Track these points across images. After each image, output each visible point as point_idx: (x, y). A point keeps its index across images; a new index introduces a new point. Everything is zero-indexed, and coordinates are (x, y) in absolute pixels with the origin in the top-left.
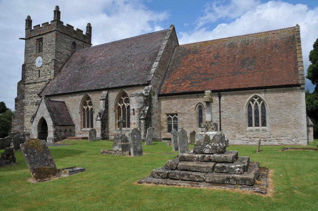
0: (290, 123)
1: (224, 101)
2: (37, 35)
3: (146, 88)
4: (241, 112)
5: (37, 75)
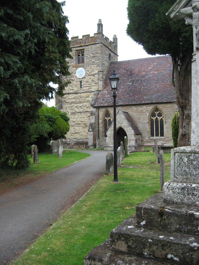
2: (76, 46)
5: (78, 86)
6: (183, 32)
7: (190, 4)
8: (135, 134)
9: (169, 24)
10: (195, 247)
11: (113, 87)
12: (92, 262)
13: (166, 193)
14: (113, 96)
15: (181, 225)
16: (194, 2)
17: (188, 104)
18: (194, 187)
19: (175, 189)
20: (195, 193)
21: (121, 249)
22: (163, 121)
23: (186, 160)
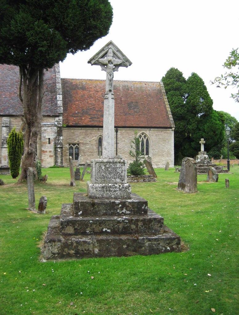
3: (57, 119)
6: (39, 46)
9: (25, 35)
10: (120, 220)
12: (52, 244)
13: (91, 192)
15: (106, 210)
17: (36, 120)
20: (111, 189)
21: (69, 232)
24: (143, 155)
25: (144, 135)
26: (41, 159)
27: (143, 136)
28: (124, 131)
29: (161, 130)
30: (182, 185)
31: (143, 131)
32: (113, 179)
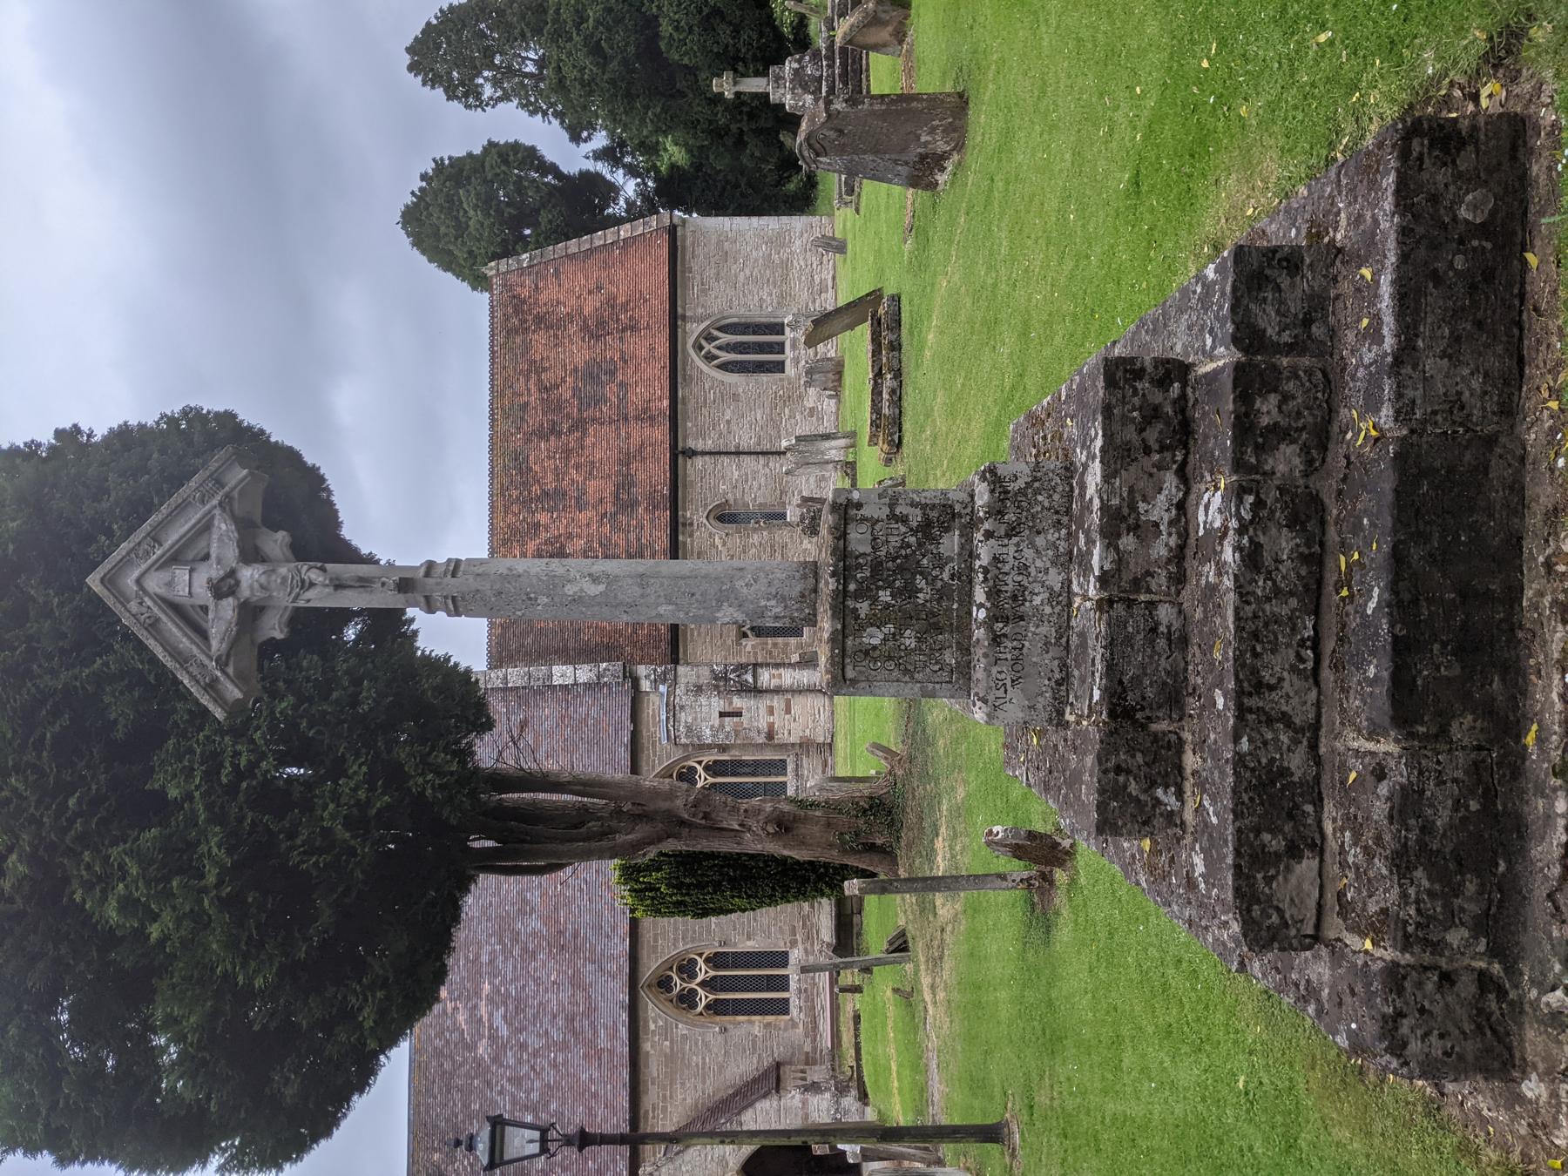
0: (775, 257)
1: (704, 439)
3: (645, 685)
4: (741, 390)
7: (197, 616)
8: (778, 1091)
10: (1238, 548)
11: (534, 1148)
14: (581, 1149)
16: (190, 593)
18: (989, 595)
19: (1003, 676)
20: (1010, 588)
22: (716, 954)
23: (874, 637)
24: (782, 345)
25: (704, 343)
26: (801, 745)
27: (707, 347)
28: (689, 424)
29: (683, 272)
30: (923, 172)
31: (691, 341)
32: (946, 576)
